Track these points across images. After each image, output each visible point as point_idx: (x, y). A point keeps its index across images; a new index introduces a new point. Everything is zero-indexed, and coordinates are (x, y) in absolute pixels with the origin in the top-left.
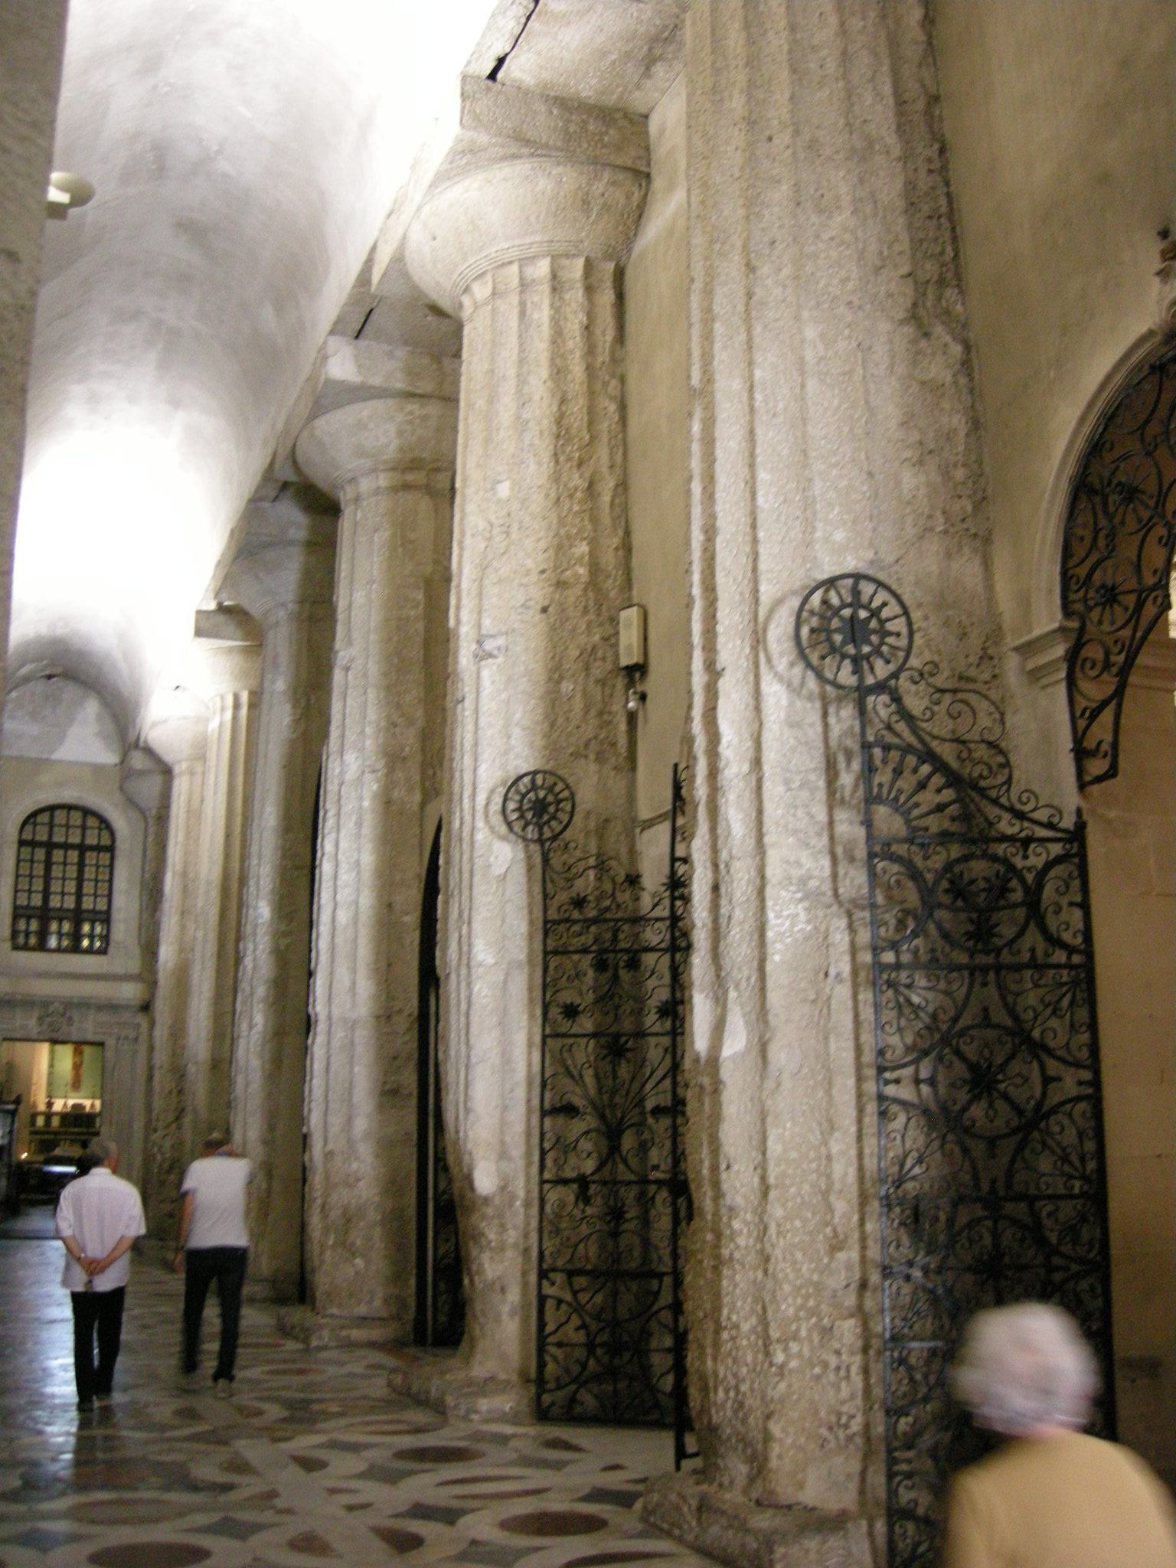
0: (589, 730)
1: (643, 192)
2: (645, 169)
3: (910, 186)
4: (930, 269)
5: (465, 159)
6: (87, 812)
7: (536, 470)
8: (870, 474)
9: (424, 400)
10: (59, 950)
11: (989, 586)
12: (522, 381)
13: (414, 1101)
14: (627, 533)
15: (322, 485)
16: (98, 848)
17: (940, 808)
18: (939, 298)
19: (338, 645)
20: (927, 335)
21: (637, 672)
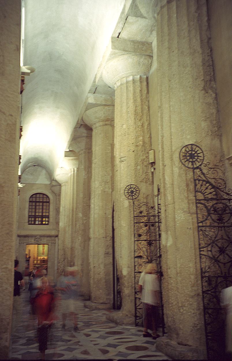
0: (144, 176)
1: (151, 60)
2: (152, 55)
3: (204, 59)
4: (208, 78)
5: (113, 56)
6: (44, 194)
7: (131, 122)
8: (195, 124)
9: (109, 106)
10: (38, 224)
11: (221, 146)
12: (127, 103)
13: (112, 255)
14: (151, 134)
15: (88, 125)
16: (46, 202)
17: (211, 193)
18: (210, 84)
19: (93, 159)
20: (207, 92)
21: (153, 164)
